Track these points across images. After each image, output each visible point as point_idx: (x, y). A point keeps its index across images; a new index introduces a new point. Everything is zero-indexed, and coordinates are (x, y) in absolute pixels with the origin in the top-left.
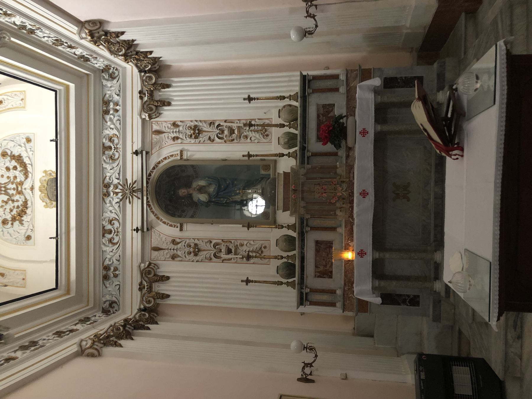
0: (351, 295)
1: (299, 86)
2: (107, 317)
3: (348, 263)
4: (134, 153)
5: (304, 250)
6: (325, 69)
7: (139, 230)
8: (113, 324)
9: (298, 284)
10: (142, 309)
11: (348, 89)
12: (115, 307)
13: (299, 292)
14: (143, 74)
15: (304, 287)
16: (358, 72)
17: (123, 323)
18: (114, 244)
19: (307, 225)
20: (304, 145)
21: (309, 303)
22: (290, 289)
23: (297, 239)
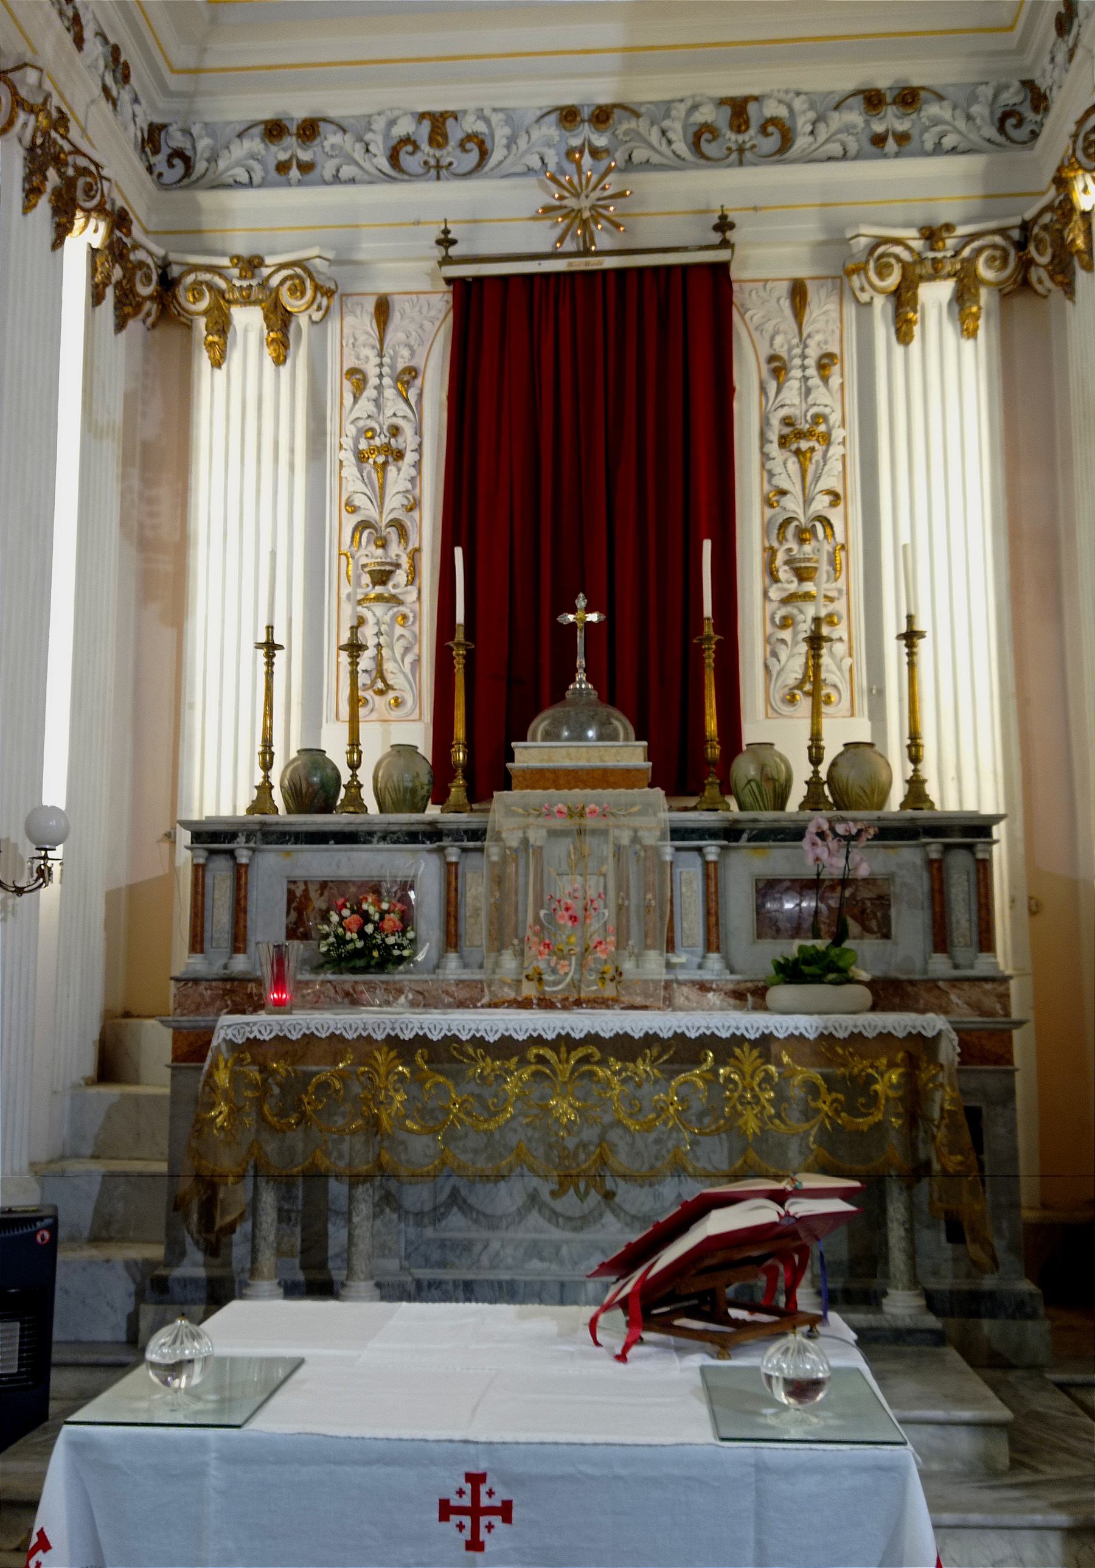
0: (229, 1002)
1: (234, 817)
2: (135, 145)
3: (336, 992)
4: (723, 217)
5: (378, 842)
6: (1033, 902)
7: (447, 248)
8: (104, 173)
9: (263, 824)
10: (168, 270)
11: (941, 984)
12: (172, 171)
13: (234, 828)
14: (1016, 234)
15: (252, 845)
16: (998, 1019)
17: (113, 210)
18: (1002, 129)
19: (948, 848)
20: (745, 836)
21: (201, 861)
22: (245, 798)
23: (876, 814)
